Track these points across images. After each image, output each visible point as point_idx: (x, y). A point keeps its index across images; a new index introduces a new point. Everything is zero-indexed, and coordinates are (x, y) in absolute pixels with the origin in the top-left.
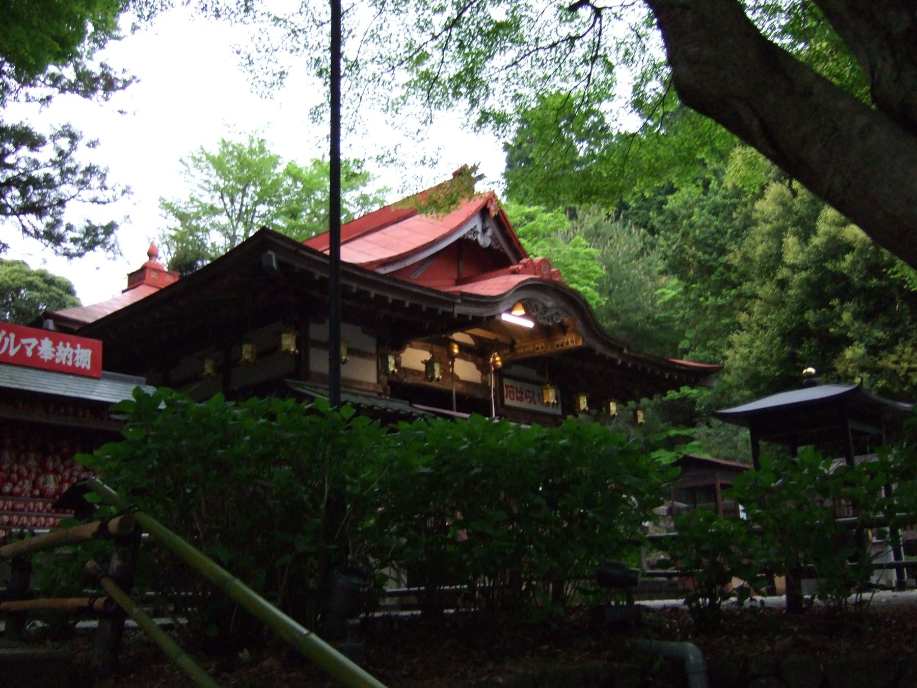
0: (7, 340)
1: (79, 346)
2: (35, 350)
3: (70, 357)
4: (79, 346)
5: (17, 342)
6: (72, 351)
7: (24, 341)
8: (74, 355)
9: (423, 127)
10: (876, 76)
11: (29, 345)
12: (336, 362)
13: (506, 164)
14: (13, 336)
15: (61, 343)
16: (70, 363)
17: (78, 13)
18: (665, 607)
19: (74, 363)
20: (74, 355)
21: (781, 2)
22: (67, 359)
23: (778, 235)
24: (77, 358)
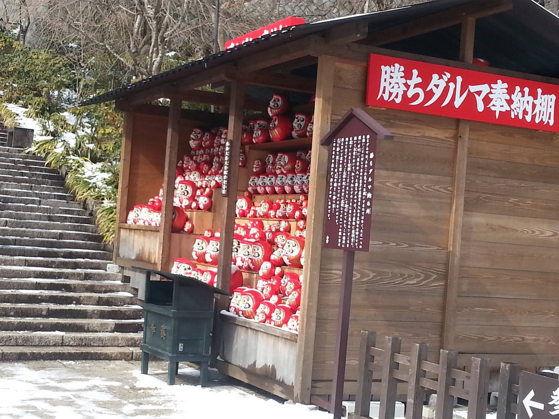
0: (452, 85)
1: (539, 91)
2: (487, 100)
3: (529, 109)
4: (539, 91)
5: (464, 88)
6: (531, 99)
7: (473, 89)
8: (534, 106)
9: (131, 284)
10: (247, 293)
11: (479, 93)
12: (349, 207)
13: (193, 386)
14: (459, 79)
15: (518, 88)
16: (528, 118)
17: (292, 339)
18: (70, 242)
19: (534, 117)
20: (534, 106)
21: (558, 369)
22: (525, 112)
23: (302, 201)
24: (537, 110)
